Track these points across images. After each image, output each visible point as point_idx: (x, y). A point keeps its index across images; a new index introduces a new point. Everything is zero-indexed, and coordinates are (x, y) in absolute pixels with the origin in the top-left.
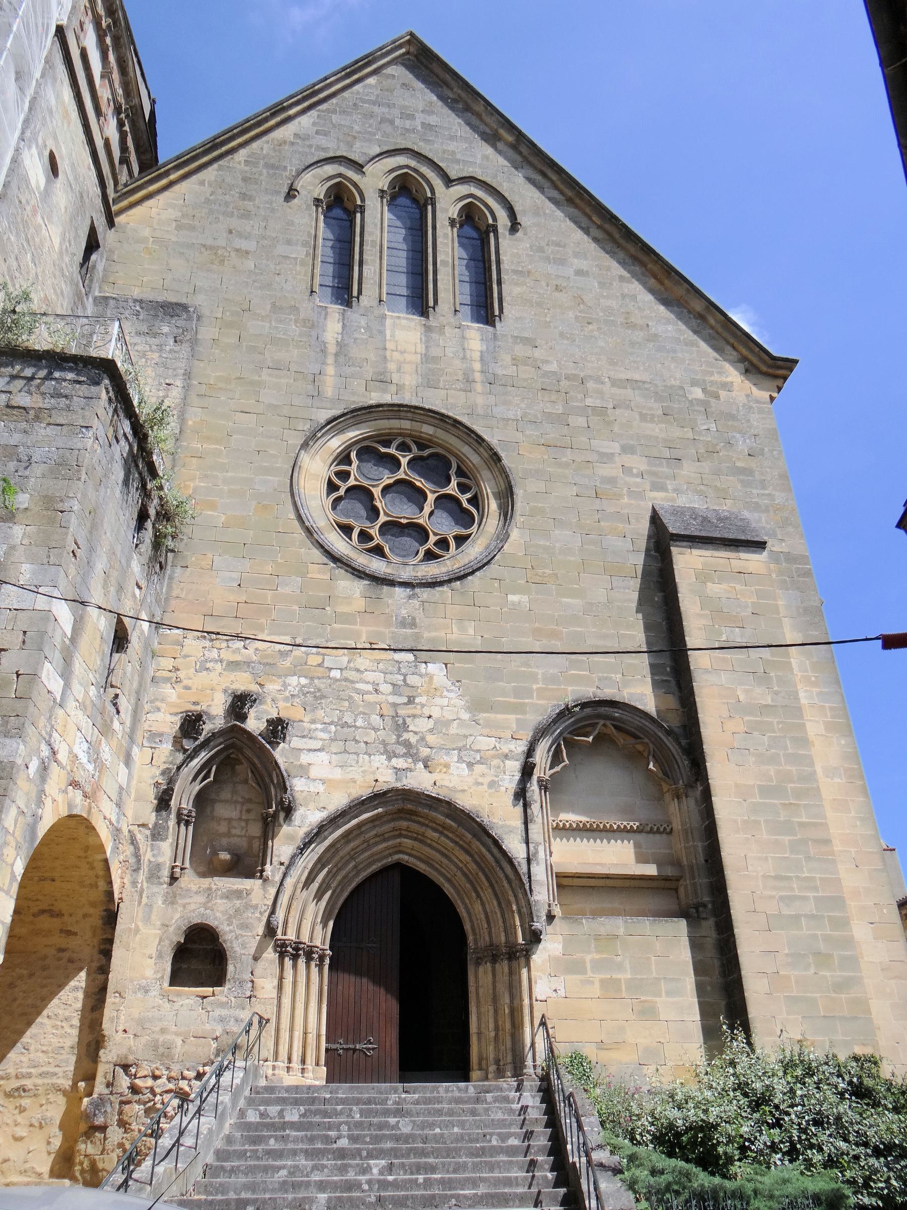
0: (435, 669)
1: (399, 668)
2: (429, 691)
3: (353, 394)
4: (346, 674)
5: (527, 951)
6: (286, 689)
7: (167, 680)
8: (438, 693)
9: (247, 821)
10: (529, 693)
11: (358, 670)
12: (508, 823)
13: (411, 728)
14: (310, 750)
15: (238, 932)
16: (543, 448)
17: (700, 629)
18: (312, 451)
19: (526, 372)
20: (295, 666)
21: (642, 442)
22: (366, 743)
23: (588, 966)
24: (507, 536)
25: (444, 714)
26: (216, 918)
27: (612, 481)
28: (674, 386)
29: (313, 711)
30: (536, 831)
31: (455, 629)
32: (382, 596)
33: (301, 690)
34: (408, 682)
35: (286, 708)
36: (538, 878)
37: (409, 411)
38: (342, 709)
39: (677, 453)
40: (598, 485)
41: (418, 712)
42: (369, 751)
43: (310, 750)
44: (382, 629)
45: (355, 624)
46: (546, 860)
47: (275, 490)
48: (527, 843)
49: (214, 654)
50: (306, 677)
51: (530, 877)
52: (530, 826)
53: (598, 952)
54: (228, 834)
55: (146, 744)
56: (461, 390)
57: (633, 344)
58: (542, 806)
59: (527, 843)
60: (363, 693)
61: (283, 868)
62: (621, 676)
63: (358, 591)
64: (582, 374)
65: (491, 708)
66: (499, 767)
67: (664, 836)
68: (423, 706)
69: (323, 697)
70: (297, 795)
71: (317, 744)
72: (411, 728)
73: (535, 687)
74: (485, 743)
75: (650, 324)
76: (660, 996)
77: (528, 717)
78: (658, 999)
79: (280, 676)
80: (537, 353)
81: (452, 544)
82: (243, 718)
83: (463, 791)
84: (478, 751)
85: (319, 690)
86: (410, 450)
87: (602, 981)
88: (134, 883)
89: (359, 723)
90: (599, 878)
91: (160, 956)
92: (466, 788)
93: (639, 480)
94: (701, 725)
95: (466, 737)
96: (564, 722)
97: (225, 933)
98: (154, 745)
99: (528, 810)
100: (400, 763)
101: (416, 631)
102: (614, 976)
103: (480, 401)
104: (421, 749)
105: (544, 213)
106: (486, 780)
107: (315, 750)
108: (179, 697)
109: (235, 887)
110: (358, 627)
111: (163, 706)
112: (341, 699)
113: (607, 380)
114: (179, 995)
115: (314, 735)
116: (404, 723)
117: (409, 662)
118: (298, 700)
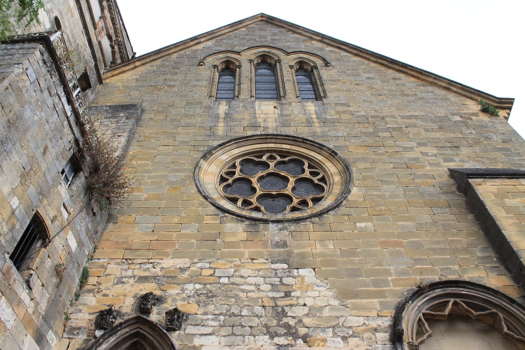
0: (306, 273)
1: (276, 274)
2: (302, 287)
3: (236, 133)
4: (232, 280)
6: (184, 292)
8: (310, 289)
10: (386, 283)
11: (242, 277)
13: (289, 314)
14: (202, 335)
16: (365, 147)
17: (511, 225)
18: (209, 160)
19: (345, 117)
20: (192, 277)
21: (430, 141)
22: (251, 327)
24: (349, 192)
25: (317, 302)
27: (416, 159)
28: (441, 116)
29: (206, 306)
31: (318, 246)
32: (259, 230)
33: (196, 292)
34: (284, 282)
35: (183, 305)
37: (273, 138)
38: (229, 303)
39: (456, 144)
40: (407, 162)
41: (294, 302)
42: (253, 333)
43: (202, 335)
44: (261, 250)
45: (240, 248)
47: (182, 179)
49: (130, 273)
50: (200, 284)
55: (65, 335)
56: (305, 126)
57: (409, 102)
60: (247, 292)
63: (241, 229)
64: (381, 115)
65: (356, 296)
66: (371, 339)
68: (298, 298)
69: (214, 296)
71: (210, 330)
72: (289, 314)
74: (355, 321)
75: (417, 94)
77: (388, 299)
79: (179, 284)
80: (350, 109)
81: (310, 204)
82: (148, 312)
84: (350, 327)
85: (211, 292)
86: (275, 158)
89: (245, 312)
93: (434, 158)
95: (338, 318)
96: (420, 301)
98: (71, 337)
101: (288, 249)
103: (318, 130)
104: (300, 329)
105: (343, 60)
107: (206, 335)
108: (98, 302)
110: (242, 250)
111: (84, 309)
112: (229, 297)
113: (398, 116)
115: (206, 323)
116: (283, 310)
117: (283, 269)
118: (193, 300)
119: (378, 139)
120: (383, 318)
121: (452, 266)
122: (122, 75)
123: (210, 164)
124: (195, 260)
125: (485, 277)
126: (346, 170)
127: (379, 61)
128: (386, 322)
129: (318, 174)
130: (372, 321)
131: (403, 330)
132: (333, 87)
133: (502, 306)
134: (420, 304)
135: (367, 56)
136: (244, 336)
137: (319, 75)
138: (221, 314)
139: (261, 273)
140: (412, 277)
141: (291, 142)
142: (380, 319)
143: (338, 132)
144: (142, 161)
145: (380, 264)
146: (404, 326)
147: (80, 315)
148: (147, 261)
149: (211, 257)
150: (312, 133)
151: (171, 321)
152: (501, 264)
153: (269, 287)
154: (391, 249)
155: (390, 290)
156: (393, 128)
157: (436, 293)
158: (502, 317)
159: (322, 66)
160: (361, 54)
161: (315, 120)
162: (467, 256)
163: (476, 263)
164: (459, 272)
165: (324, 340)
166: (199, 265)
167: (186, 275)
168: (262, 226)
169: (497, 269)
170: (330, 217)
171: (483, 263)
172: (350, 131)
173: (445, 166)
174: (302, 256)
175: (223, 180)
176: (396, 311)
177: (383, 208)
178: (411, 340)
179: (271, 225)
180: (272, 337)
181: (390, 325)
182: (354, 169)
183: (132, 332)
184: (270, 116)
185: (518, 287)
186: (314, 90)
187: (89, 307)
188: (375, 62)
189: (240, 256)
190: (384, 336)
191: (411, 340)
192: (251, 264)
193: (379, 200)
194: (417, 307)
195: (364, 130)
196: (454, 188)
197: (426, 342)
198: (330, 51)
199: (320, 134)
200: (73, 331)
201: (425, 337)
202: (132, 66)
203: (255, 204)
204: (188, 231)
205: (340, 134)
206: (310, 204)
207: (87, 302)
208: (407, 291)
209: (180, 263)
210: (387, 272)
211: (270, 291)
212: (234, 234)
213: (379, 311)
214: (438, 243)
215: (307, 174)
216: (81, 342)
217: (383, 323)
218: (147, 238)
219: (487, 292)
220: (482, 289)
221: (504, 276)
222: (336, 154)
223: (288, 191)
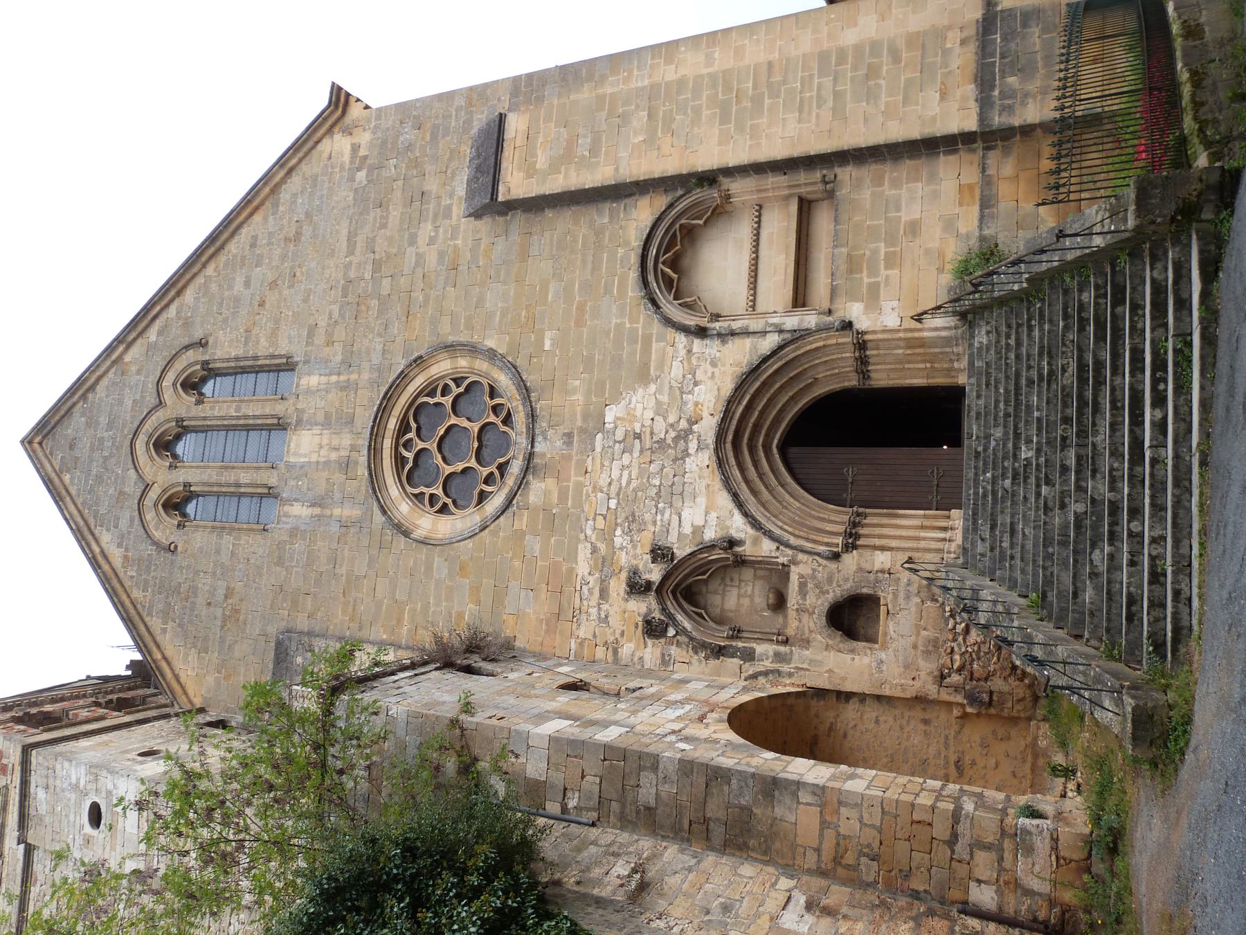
4: (613, 494)
5: (858, 333)
7: (615, 652)
9: (740, 581)
11: (610, 484)
12: (748, 350)
14: (680, 526)
15: (835, 585)
17: (578, 175)
22: (675, 476)
23: (873, 280)
26: (822, 604)
27: (441, 255)
30: (755, 325)
31: (575, 398)
36: (796, 324)
43: (680, 526)
48: (766, 332)
49: (594, 611)
51: (795, 331)
52: (751, 330)
53: (861, 272)
54: (751, 597)
56: (356, 393)
59: (766, 332)
61: (781, 547)
66: (699, 358)
67: (762, 211)
68: (643, 426)
69: (633, 515)
70: (719, 536)
71: (675, 518)
73: (628, 326)
76: (900, 217)
77: (655, 332)
78: (903, 220)
79: (614, 553)
81: (497, 401)
82: (649, 584)
83: (719, 390)
85: (627, 518)
87: (886, 268)
88: (790, 675)
91: (852, 651)
92: (716, 387)
93: (441, 230)
97: (835, 596)
100: (693, 446)
103: (366, 376)
106: (710, 369)
108: (630, 641)
109: (797, 588)
111: (638, 654)
114: (885, 634)
119: (395, 297)
122: (182, 680)
123: (417, 527)
124: (582, 536)
126: (451, 348)
127: (204, 259)
128: (681, 339)
129: (446, 386)
132: (263, 342)
135: (188, 276)
136: (685, 483)
137: (223, 360)
138: (656, 507)
139: (607, 463)
141: (386, 415)
143: (374, 349)
144: (404, 618)
145: (607, 333)
146: (692, 323)
147: (647, 657)
148: (578, 592)
149: (579, 519)
150: (372, 386)
151: (664, 556)
153: (626, 456)
154: (587, 317)
156: (374, 271)
159: (203, 353)
160: (180, 285)
161: (342, 378)
162: (607, 234)
165: (696, 404)
166: (589, 532)
167: (602, 547)
168: (536, 460)
170: (531, 379)
172: (373, 332)
173: (459, 220)
174: (586, 417)
175: (444, 510)
177: (524, 313)
179: (536, 450)
180: (688, 455)
182: (451, 339)
183: (671, 597)
184: (325, 441)
186: (236, 374)
187: (637, 648)
188: (204, 266)
189: (580, 486)
190: (697, 344)
192: (593, 474)
193: (510, 316)
195: (374, 313)
196: (500, 219)
198: (160, 333)
199: (376, 374)
200: (665, 661)
202: (164, 664)
203: (493, 468)
204: (537, 547)
205: (379, 347)
206: (497, 401)
207: (630, 652)
209: (584, 552)
210: (619, 327)
211: (631, 454)
212: (547, 493)
214: (584, 261)
215: (447, 401)
216: (679, 650)
218: (543, 596)
222: (421, 357)
223: (475, 427)
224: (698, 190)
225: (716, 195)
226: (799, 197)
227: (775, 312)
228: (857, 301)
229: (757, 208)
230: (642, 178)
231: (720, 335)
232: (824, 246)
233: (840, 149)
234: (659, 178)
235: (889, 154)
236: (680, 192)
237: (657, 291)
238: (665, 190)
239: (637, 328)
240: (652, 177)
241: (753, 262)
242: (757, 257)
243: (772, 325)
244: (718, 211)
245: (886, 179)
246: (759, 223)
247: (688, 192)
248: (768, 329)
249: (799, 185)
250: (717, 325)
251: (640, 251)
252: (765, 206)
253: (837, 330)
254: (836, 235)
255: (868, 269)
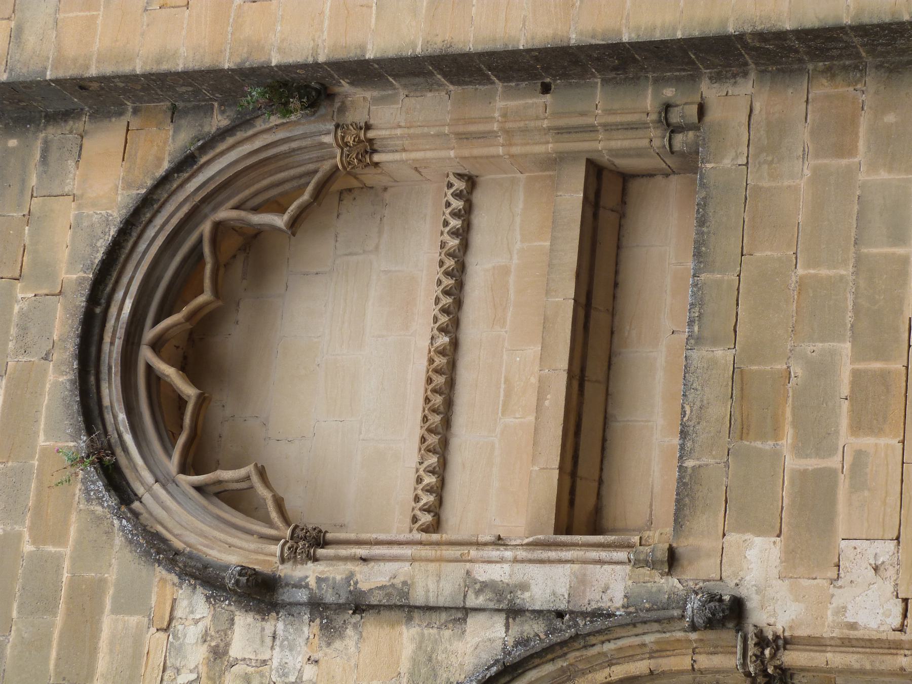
5: (762, 641)
23: (812, 463)
46: (516, 560)
48: (467, 611)
51: (560, 615)
52: (418, 597)
53: (776, 432)
58: (364, 560)
59: (467, 611)
62: (19, 285)
67: (479, 197)
73: (28, 547)
77: (111, 576)
87: (857, 427)
90: (580, 404)
94: (165, 67)
96: (135, 468)
99: (374, 601)
102: (845, 390)
120: (179, 613)
121: (16, 308)
125: (79, 207)
130: (184, 657)
131: (244, 570)
133: (198, 198)
134: (148, 477)
140: (36, 463)
142: (180, 627)
146: (233, 559)
152: (38, 130)
155: (76, 559)
157: (116, 405)
158: (234, 214)
163: (17, 215)
164: (46, 291)
169: (54, 156)
171: (22, 191)
176: (159, 562)
178: (277, 549)
181: (208, 598)
185: (136, 111)
191: (277, 549)
194: (157, 487)
197: (281, 494)
201: (261, 491)
208: (89, 500)
213: (151, 622)
217: (196, 622)
219: (140, 228)
220: (127, 241)
221: (86, 142)
224: (275, 120)
225: (328, 139)
226: (590, 163)
227: (499, 542)
228: (760, 533)
229: (460, 185)
230: (93, 72)
231: (317, 606)
232: (667, 324)
233: (713, 30)
234: (149, 76)
235: (872, 52)
236: (219, 121)
237: (128, 438)
238: (174, 109)
239: (59, 558)
240: (126, 69)
241: (440, 361)
242: (455, 344)
243: (485, 586)
244: (336, 186)
245: (862, 130)
246: (464, 234)
247: (243, 122)
248: (473, 601)
249: (591, 129)
250: (310, 572)
251: (81, 301)
252: (487, 178)
253: (694, 627)
254: (698, 302)
255: (795, 424)
